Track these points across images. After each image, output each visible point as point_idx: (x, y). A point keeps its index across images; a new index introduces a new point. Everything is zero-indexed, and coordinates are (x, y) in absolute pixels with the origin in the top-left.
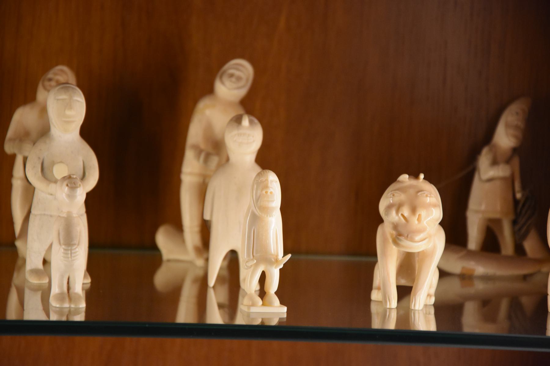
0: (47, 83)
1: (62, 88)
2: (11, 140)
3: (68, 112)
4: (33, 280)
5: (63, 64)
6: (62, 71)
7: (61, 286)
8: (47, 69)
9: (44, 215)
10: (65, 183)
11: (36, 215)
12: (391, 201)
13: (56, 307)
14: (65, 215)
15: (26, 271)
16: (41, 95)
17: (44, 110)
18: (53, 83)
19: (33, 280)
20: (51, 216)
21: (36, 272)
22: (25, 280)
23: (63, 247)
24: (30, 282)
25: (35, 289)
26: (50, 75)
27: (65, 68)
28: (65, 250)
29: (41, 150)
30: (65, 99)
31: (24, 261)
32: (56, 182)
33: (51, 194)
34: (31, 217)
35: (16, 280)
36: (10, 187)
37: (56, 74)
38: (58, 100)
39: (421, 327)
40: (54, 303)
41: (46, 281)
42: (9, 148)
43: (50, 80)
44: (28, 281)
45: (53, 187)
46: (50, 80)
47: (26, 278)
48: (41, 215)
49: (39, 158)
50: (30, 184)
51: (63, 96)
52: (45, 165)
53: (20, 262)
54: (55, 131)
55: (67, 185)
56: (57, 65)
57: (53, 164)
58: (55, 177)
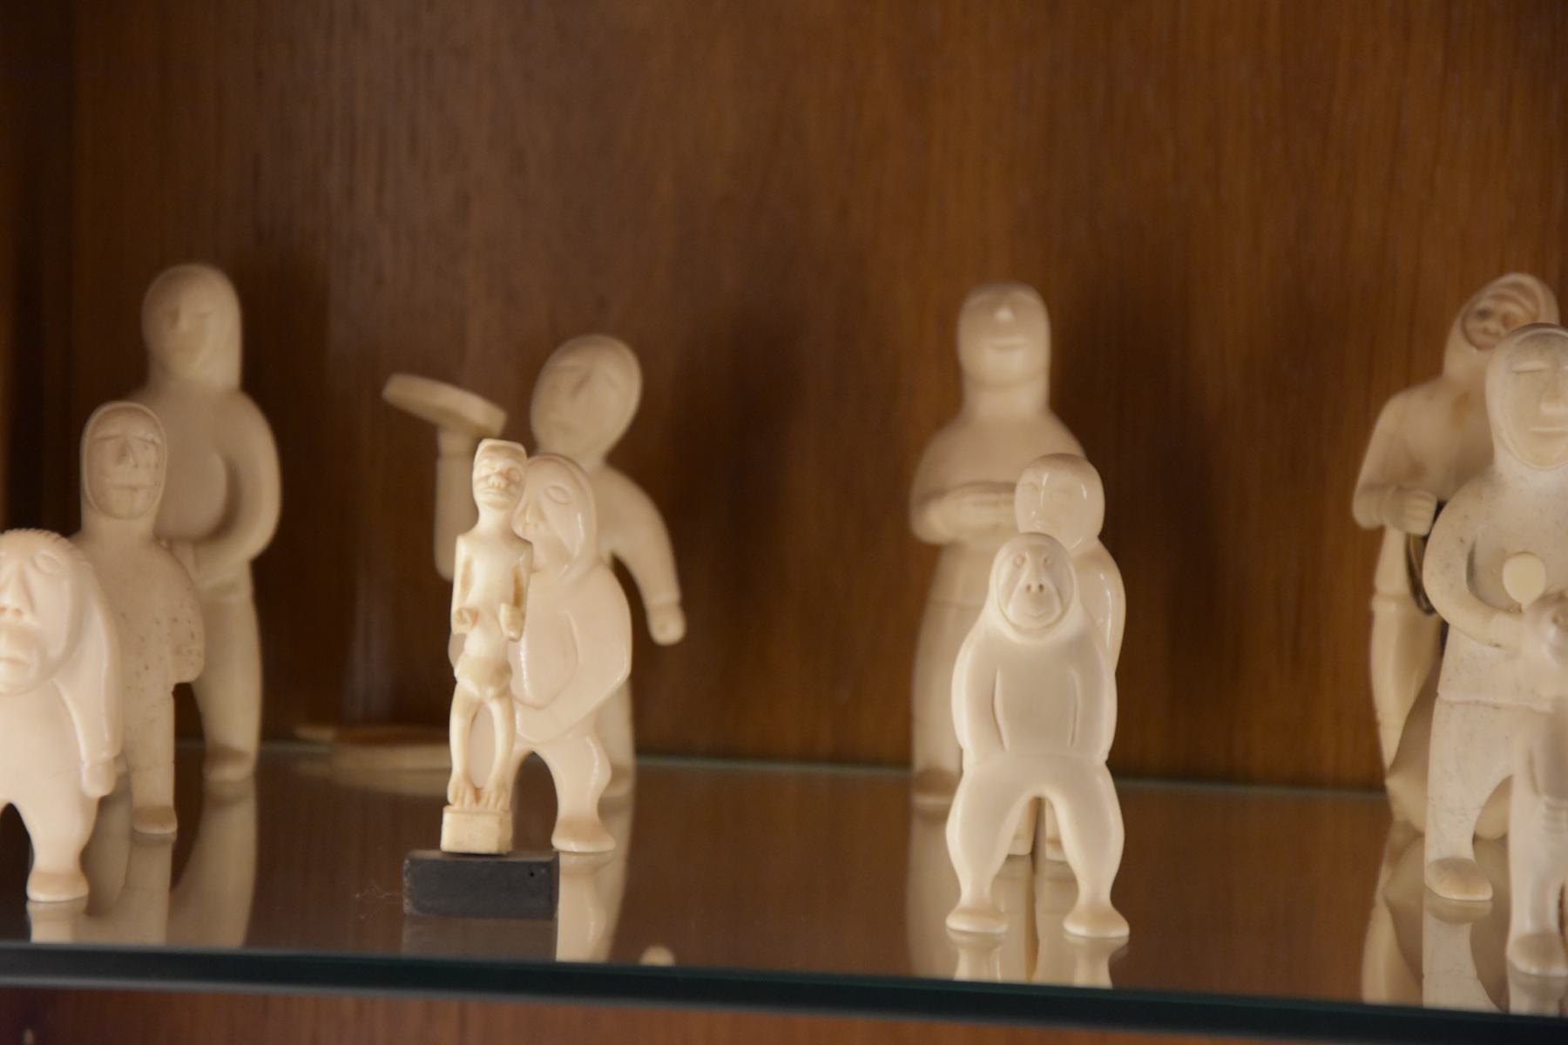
0: (1475, 325)
1: (1533, 338)
2: (1371, 487)
3: (1548, 409)
4: (1449, 892)
5: (1519, 269)
6: (1518, 287)
7: (1538, 914)
8: (1470, 286)
9: (1477, 703)
10: (1548, 615)
11: (1452, 705)
12: (1045, 477)
13: (1527, 975)
14: (1546, 707)
15: (1426, 864)
16: (1459, 359)
17: (1470, 402)
18: (1492, 325)
19: (1449, 892)
20: (1496, 707)
21: (1453, 867)
22: (1421, 891)
23: (1546, 798)
24: (1440, 897)
25: (1454, 916)
26: (1485, 302)
27: (1528, 280)
28: (1549, 807)
29: (1466, 517)
30: (1540, 371)
31: (1418, 836)
32: (1514, 610)
33: (1497, 646)
34: (1439, 709)
35: (1389, 885)
36: (1366, 621)
37: (1500, 298)
38: (1518, 373)
39: (596, 771)
40: (1520, 961)
41: (1484, 895)
42: (1364, 512)
43: (1484, 314)
44: (1432, 893)
45: (1502, 625)
46: (1484, 314)
47: (1427, 883)
48: (1468, 703)
49: (1462, 541)
50: (1430, 610)
51: (1534, 363)
52: (1480, 560)
53: (1396, 836)
54: (1510, 461)
55: (1555, 621)
56: (1502, 271)
57: (1502, 556)
58: (1507, 595)
